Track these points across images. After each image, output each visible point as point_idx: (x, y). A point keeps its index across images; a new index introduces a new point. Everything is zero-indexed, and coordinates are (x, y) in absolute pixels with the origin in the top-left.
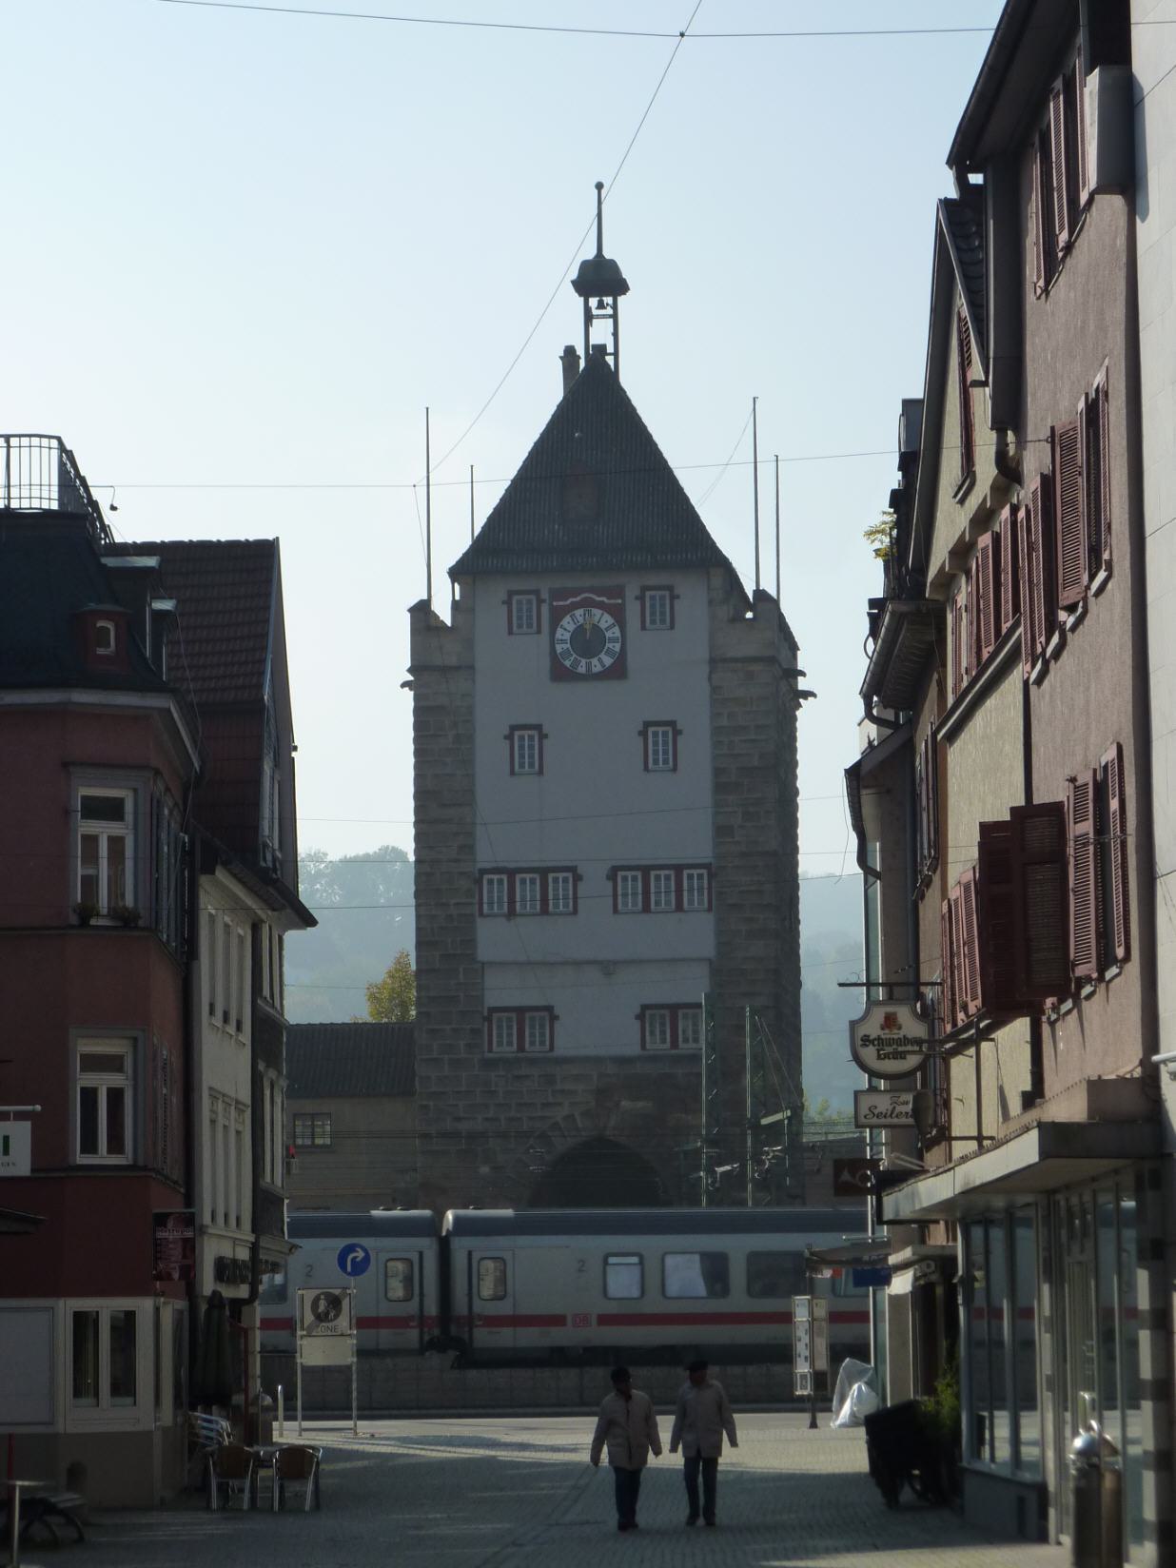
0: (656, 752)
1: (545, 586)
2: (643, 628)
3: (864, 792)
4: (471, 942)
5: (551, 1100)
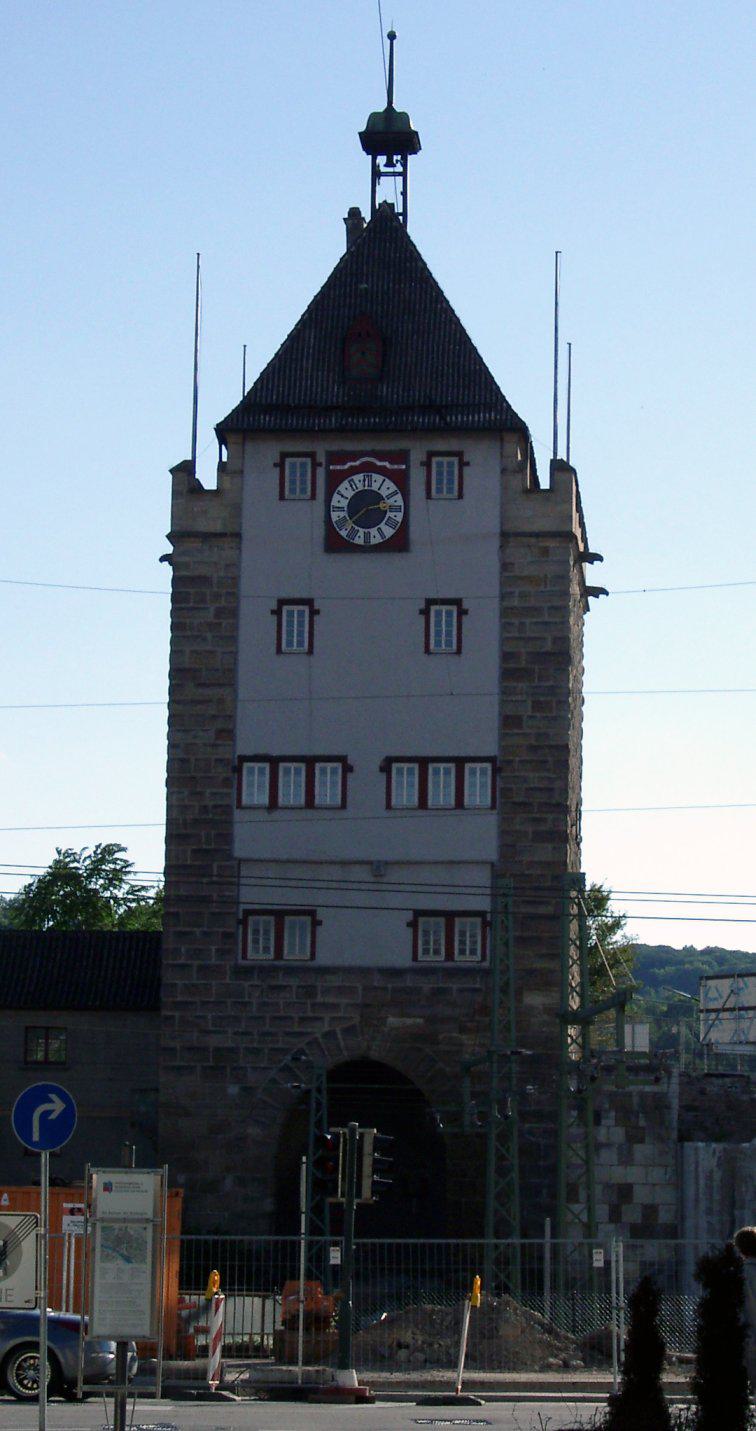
0: (438, 634)
1: (321, 449)
2: (429, 496)
3: (401, 211)
4: (227, 838)
5: (310, 1014)
